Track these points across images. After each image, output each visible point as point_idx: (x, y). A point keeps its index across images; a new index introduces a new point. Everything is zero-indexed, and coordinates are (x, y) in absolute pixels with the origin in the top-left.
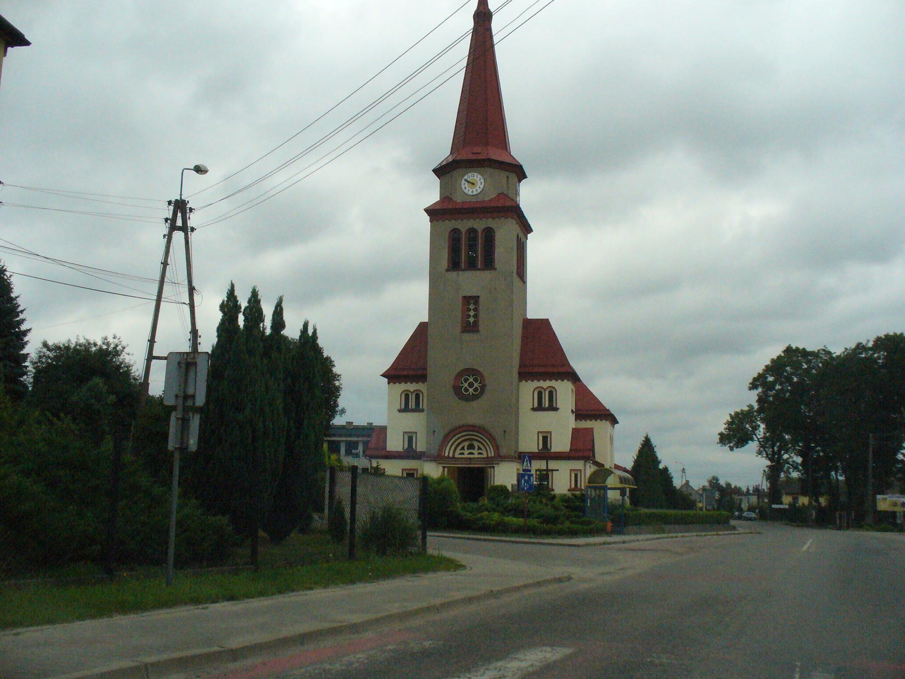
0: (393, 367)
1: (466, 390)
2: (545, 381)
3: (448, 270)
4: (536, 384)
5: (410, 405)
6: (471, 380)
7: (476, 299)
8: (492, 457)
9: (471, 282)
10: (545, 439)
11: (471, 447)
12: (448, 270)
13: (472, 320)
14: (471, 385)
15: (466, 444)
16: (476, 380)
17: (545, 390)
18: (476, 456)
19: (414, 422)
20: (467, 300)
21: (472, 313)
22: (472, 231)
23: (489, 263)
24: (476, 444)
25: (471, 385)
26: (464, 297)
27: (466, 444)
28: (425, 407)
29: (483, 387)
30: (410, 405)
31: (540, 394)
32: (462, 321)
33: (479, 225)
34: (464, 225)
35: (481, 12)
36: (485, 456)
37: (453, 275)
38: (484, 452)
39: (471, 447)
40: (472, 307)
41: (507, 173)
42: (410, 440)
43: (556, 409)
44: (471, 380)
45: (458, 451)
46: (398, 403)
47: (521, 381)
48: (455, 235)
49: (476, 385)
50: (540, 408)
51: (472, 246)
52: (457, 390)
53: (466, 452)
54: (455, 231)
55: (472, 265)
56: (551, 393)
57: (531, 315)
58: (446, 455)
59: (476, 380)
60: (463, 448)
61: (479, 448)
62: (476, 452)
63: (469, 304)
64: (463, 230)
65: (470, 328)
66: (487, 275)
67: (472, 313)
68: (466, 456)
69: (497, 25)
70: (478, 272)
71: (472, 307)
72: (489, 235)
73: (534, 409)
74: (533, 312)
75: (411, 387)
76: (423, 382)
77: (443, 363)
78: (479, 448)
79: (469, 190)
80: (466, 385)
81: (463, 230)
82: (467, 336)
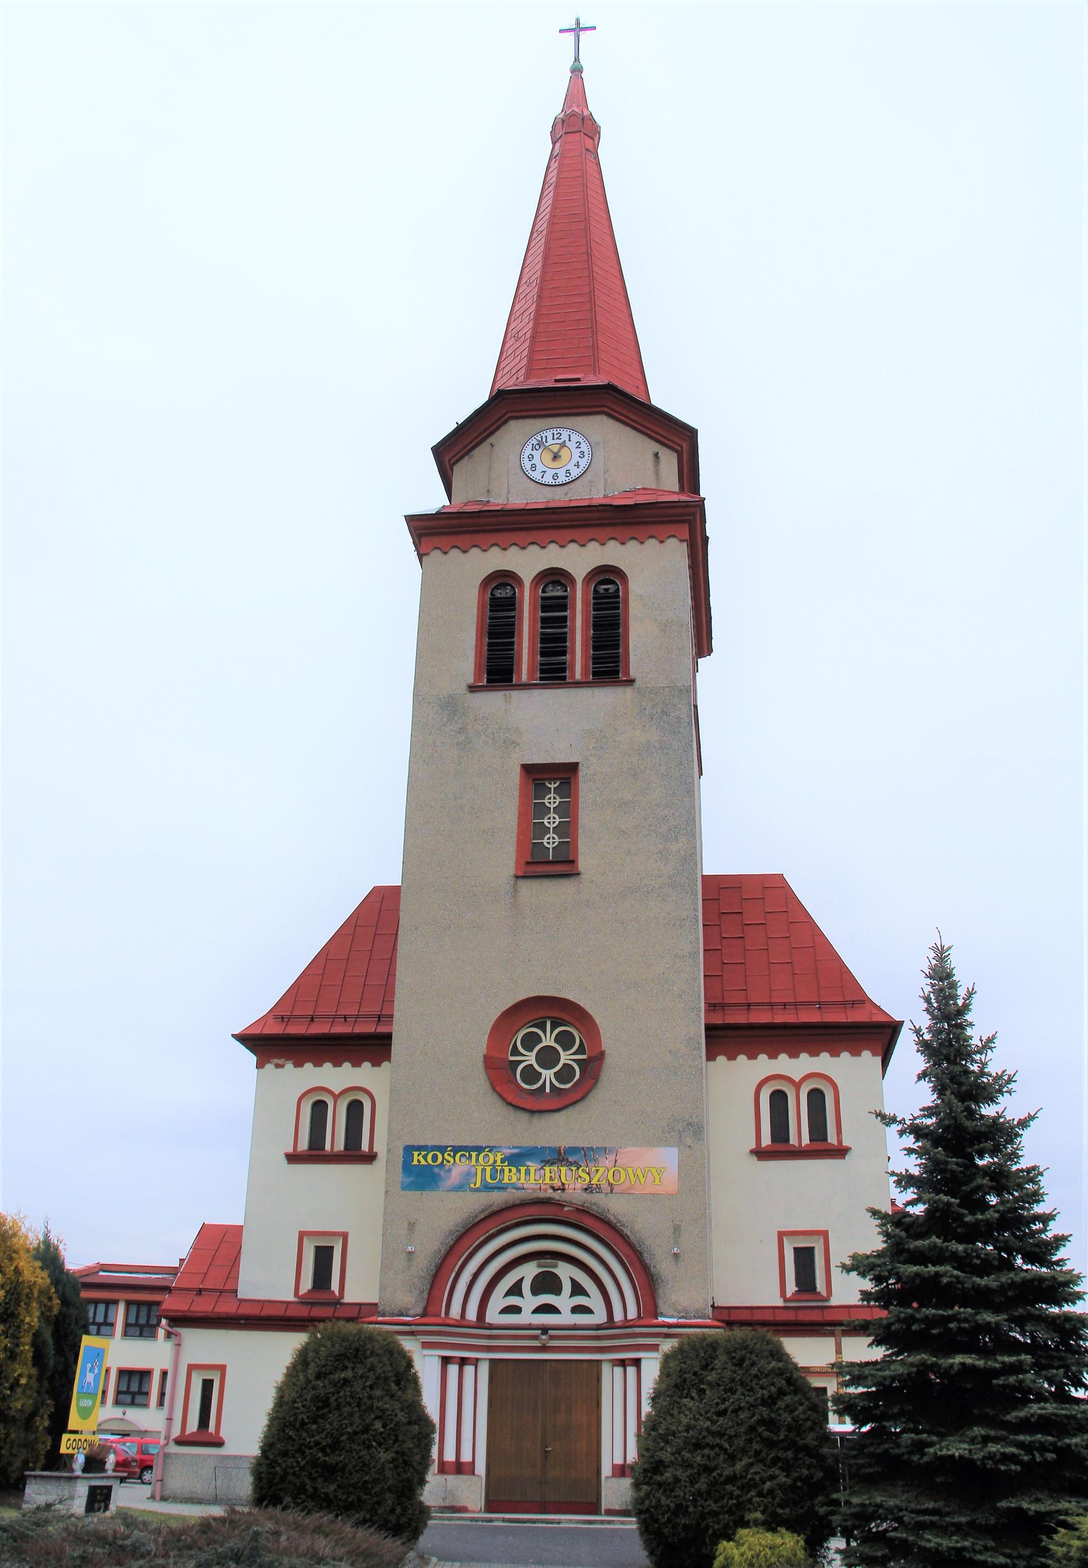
0: (279, 1013)
1: (531, 1075)
2: (794, 1055)
3: (473, 689)
4: (764, 1066)
5: (329, 1141)
6: (548, 1040)
7: (565, 774)
8: (627, 1324)
9: (548, 720)
10: (323, 1256)
11: (547, 1283)
12: (473, 689)
13: (550, 841)
14: (548, 1058)
15: (529, 1271)
16: (565, 1040)
17: (797, 1086)
18: (566, 1318)
19: (348, 1200)
20: (537, 775)
21: (552, 821)
22: (555, 577)
23: (609, 666)
24: (565, 1272)
25: (548, 1058)
26: (528, 769)
27: (529, 1271)
28: (380, 1147)
29: (593, 1064)
30: (329, 1141)
31: (779, 1100)
32: (520, 844)
33: (579, 559)
34: (527, 562)
35: (573, 115)
36: (599, 1317)
37: (494, 701)
38: (595, 1301)
39: (547, 1283)
40: (552, 801)
41: (655, 447)
42: (323, 1256)
43: (841, 1152)
44: (548, 1040)
45: (498, 1300)
46: (288, 1130)
47: (711, 1056)
48: (499, 598)
49: (566, 1057)
50: (778, 1148)
51: (553, 644)
52: (499, 1070)
53: (529, 1301)
54: (503, 579)
55: (553, 673)
56: (816, 1097)
57: (709, 870)
58: (455, 1311)
59: (565, 1040)
60: (516, 1290)
61: (577, 1289)
62: (564, 1301)
63: (540, 790)
64: (527, 576)
65: (548, 861)
66: (605, 697)
67: (552, 821)
68: (526, 1317)
69: (610, 154)
70: (573, 692)
71: (552, 801)
72: (608, 588)
73: (761, 1154)
74: (728, 849)
75: (336, 1077)
76: (376, 1063)
77: (443, 1013)
78: (577, 1289)
79: (543, 469)
80: (530, 1058)
81: (527, 576)
82: (531, 890)
